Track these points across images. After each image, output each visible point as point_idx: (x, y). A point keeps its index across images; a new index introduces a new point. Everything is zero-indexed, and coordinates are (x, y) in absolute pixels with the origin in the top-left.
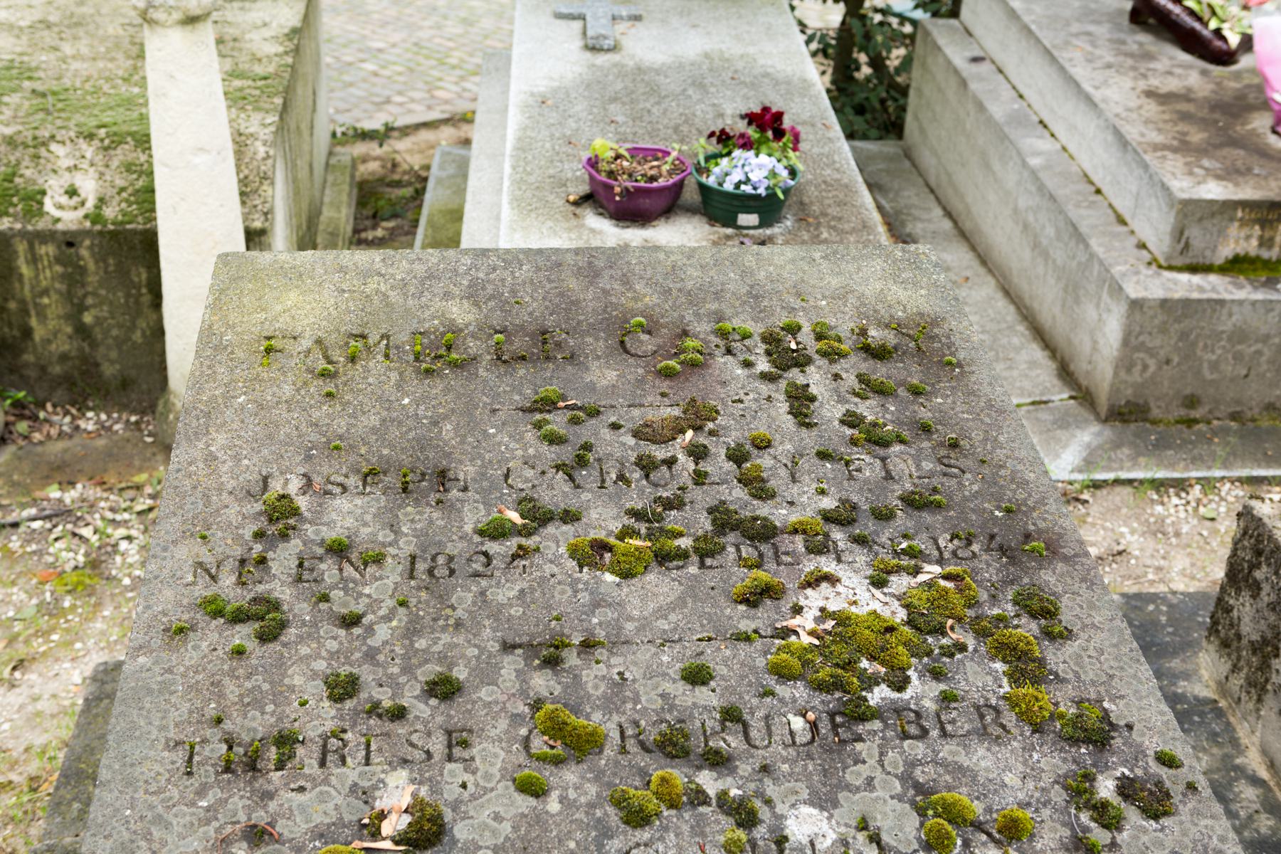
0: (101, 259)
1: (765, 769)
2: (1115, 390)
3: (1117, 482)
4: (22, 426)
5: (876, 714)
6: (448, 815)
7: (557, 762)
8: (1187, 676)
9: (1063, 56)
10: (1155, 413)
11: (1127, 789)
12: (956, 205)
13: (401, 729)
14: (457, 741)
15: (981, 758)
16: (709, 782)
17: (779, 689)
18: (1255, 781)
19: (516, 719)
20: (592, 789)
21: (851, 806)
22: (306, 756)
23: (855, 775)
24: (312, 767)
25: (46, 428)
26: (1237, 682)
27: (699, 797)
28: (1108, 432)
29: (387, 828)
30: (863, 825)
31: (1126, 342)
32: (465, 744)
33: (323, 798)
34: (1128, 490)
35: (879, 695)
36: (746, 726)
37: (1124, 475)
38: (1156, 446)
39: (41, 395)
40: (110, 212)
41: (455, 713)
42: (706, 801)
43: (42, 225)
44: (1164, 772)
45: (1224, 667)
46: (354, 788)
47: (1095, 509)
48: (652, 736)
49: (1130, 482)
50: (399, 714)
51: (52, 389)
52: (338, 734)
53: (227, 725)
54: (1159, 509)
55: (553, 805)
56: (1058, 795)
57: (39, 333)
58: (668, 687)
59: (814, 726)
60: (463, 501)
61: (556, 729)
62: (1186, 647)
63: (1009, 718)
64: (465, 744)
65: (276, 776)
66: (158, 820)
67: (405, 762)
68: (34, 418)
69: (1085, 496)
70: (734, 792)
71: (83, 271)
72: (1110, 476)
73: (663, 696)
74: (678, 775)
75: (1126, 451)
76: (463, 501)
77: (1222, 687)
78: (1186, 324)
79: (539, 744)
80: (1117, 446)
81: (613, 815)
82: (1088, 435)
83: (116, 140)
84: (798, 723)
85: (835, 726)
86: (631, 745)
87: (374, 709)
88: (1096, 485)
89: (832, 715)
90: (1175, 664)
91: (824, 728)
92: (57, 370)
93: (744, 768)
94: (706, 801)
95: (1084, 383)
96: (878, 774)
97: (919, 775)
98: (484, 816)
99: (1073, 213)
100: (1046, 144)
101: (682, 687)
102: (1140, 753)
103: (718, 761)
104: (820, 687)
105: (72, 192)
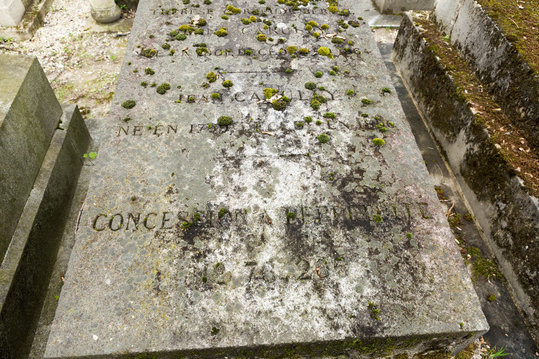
1: (274, 17)
2: (385, 5)
3: (382, 27)
4: (125, 14)
5: (299, 9)
6: (207, 22)
7: (231, 14)
8: (387, 58)
10: (394, 12)
11: (350, 23)
13: (198, 9)
14: (210, 11)
15: (321, 17)
16: (262, 18)
17: (279, 5)
18: (398, 77)
19: (222, 8)
20: (237, 19)
21: (291, 23)
22: (179, 13)
23: (292, 18)
24: (180, 14)
25: (131, 15)
26: (398, 56)
27: (260, 21)
28: (382, 16)
29: (194, 23)
30: (293, 26)
32: (211, 11)
33: (181, 18)
34: (384, 29)
35: (301, 7)
36: (271, 11)
37: (384, 26)
38: (393, 20)
39: (129, 7)
41: (210, 7)
42: (261, 21)
44: (359, 21)
45: (396, 54)
46: (188, 17)
47: (376, 33)
48: (251, 11)
49: (385, 27)
50: (198, 6)
51: (132, 6)
52: (185, 9)
53: (162, 7)
54: (391, 34)
55: (229, 21)
56: (335, 23)
58: (255, 4)
59: (286, 11)
60: (263, 142)
61: (230, 9)
62: (389, 52)
63: (328, 11)
64: (211, 11)
65: (172, 15)
66: (148, 21)
67: (199, 14)
68: (128, 13)
69: (374, 30)
70: (267, 20)
72: (380, 26)
73: (254, 5)
74: (256, 17)
75: (386, 20)
76: (263, 142)
77: (395, 60)
79: (227, 12)
80: (383, 19)
81: (241, 23)
82: (378, 17)
84: (282, 11)
85: (290, 11)
86: (246, 13)
87: (193, 6)
88: (377, 28)
89: (290, 10)
90: (385, 56)
91: (288, 11)
93: (269, 17)
94: (261, 21)
95: (378, 5)
96: (298, 19)
97: (306, 19)
98: (215, 22)
101: (258, 4)
102: (355, 18)
103: (264, 15)
104: (288, 5)
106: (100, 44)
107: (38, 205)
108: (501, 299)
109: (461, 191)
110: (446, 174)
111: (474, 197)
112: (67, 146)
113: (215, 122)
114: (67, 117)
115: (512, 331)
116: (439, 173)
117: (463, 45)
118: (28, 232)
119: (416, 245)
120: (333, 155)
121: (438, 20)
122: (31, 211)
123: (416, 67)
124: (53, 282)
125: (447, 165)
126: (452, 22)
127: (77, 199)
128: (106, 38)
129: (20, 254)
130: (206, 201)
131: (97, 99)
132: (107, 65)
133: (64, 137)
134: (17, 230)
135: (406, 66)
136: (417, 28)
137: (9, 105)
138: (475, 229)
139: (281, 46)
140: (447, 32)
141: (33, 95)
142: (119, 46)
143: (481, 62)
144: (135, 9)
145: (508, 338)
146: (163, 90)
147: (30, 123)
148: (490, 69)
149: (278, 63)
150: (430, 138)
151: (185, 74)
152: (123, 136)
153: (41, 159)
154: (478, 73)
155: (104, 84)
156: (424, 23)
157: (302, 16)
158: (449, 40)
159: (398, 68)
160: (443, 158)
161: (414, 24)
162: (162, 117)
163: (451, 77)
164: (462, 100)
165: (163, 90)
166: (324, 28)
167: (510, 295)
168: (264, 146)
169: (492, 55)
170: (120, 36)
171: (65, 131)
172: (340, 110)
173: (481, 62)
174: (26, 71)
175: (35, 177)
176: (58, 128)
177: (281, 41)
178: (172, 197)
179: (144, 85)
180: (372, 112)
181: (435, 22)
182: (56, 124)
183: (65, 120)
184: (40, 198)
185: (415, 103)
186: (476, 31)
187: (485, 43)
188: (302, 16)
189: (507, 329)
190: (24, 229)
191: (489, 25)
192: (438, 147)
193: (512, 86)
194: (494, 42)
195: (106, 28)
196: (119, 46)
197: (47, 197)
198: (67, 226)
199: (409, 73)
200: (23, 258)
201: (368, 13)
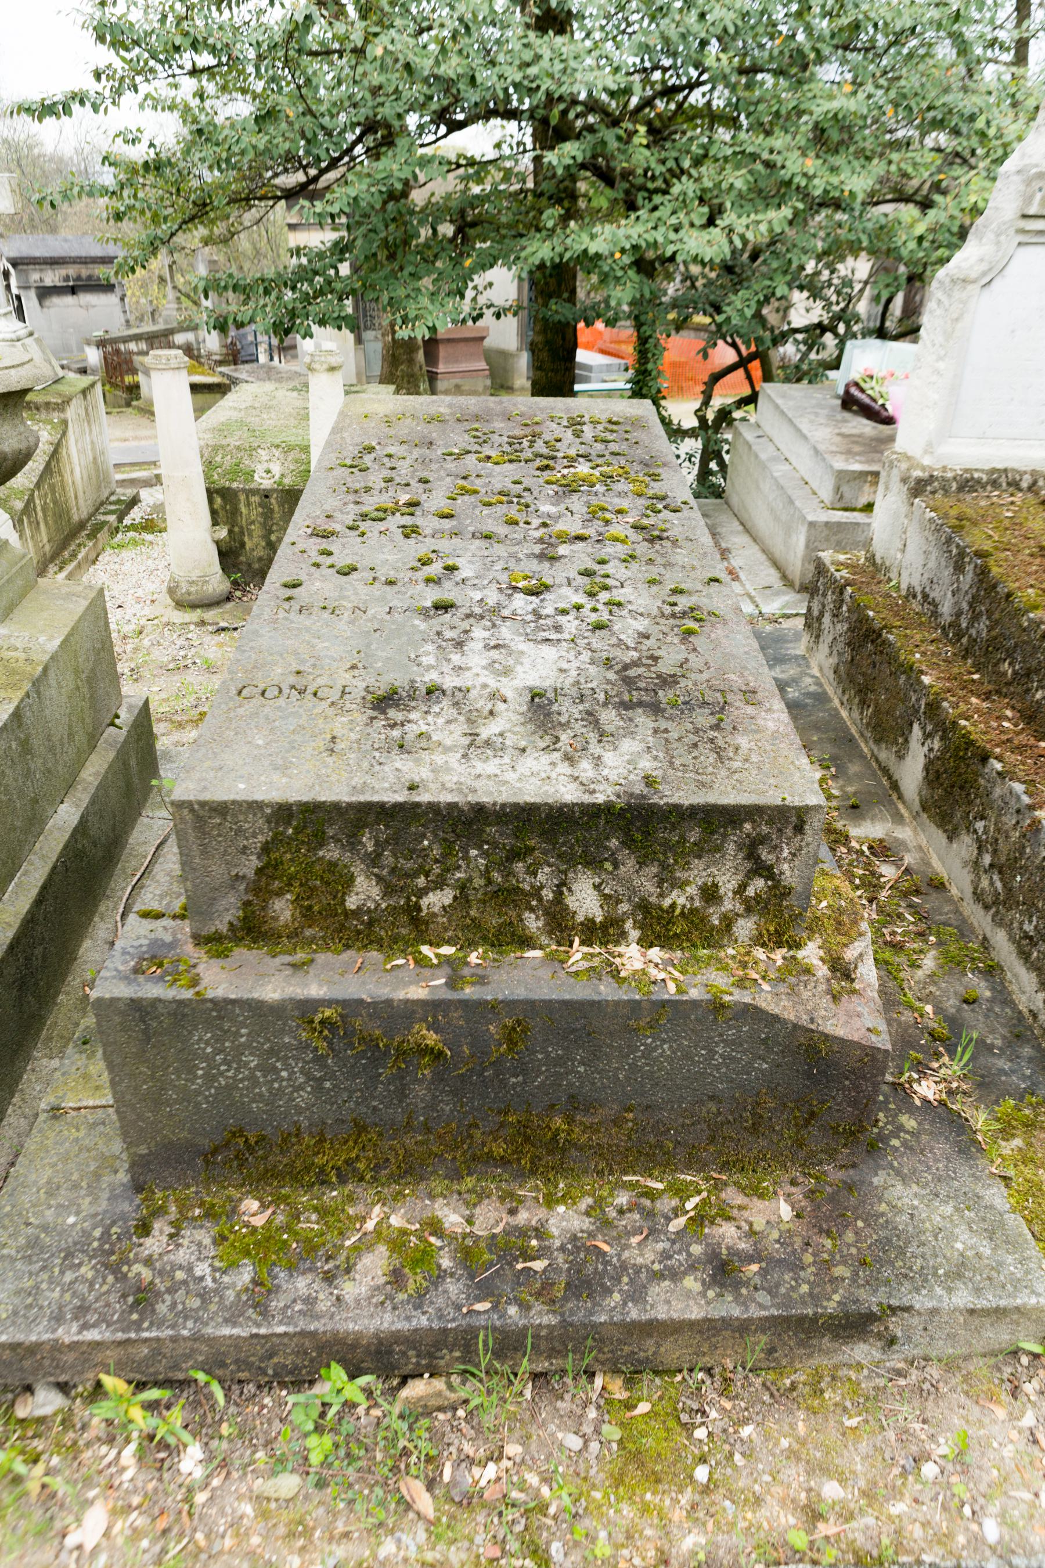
0: (281, 505)
2: (803, 574)
4: (238, 594)
9: (797, 421)
12: (745, 517)
21: (563, 506)
22: (375, 492)
31: (807, 546)
40: (287, 481)
43: (253, 486)
57: (249, 545)
71: (272, 511)
78: (839, 536)
83: (289, 449)
92: (256, 566)
99: (790, 492)
100: (786, 467)
105: (268, 472)
106: (180, 642)
107: (70, 830)
108: (992, 1000)
109: (924, 843)
110: (898, 818)
111: (940, 837)
112: (122, 757)
113: (429, 604)
114: (130, 707)
115: (1009, 1045)
116: (883, 819)
117: (918, 589)
118: (50, 865)
119: (730, 728)
120: (614, 641)
121: (878, 561)
122: (56, 834)
123: (840, 646)
124: (68, 993)
125: (900, 806)
126: (899, 556)
127: (124, 869)
128: (194, 633)
129: (34, 892)
130: (408, 677)
131: (172, 721)
132: (192, 677)
133: (121, 739)
134: (32, 857)
135: (827, 651)
136: (838, 575)
137: (57, 642)
138: (950, 900)
139: (543, 530)
140: (893, 575)
141: (88, 645)
142: (220, 645)
143: (946, 609)
144: (260, 584)
145: (1000, 1056)
146: (347, 572)
147: (78, 688)
148: (959, 614)
149: (537, 549)
150: (870, 767)
151: (382, 557)
152: (282, 614)
153: (80, 763)
154: (943, 628)
155: (191, 700)
156: (852, 567)
157: (584, 499)
158: (898, 588)
159: (814, 663)
160: (895, 797)
161: (832, 569)
162: (344, 598)
163: (891, 637)
164: (909, 669)
165: (347, 572)
166: (620, 512)
167: (1010, 994)
168: (504, 630)
169: (958, 589)
170: (224, 629)
171: (124, 732)
172: (632, 598)
173: (946, 609)
174: (86, 603)
175: (70, 785)
176: (112, 724)
177: (545, 525)
178: (356, 672)
179: (317, 565)
180: (684, 602)
181: (874, 564)
182: (110, 715)
183: (126, 717)
184: (75, 820)
185: (844, 714)
186: (933, 557)
187: (947, 573)
188: (584, 499)
189: (998, 1042)
190: (43, 857)
191: (949, 541)
192: (885, 782)
193: (990, 629)
194: (959, 568)
195: (195, 615)
196: (220, 645)
197: (81, 829)
198: (102, 908)
199: (833, 660)
200: (39, 902)
201: (768, 592)
